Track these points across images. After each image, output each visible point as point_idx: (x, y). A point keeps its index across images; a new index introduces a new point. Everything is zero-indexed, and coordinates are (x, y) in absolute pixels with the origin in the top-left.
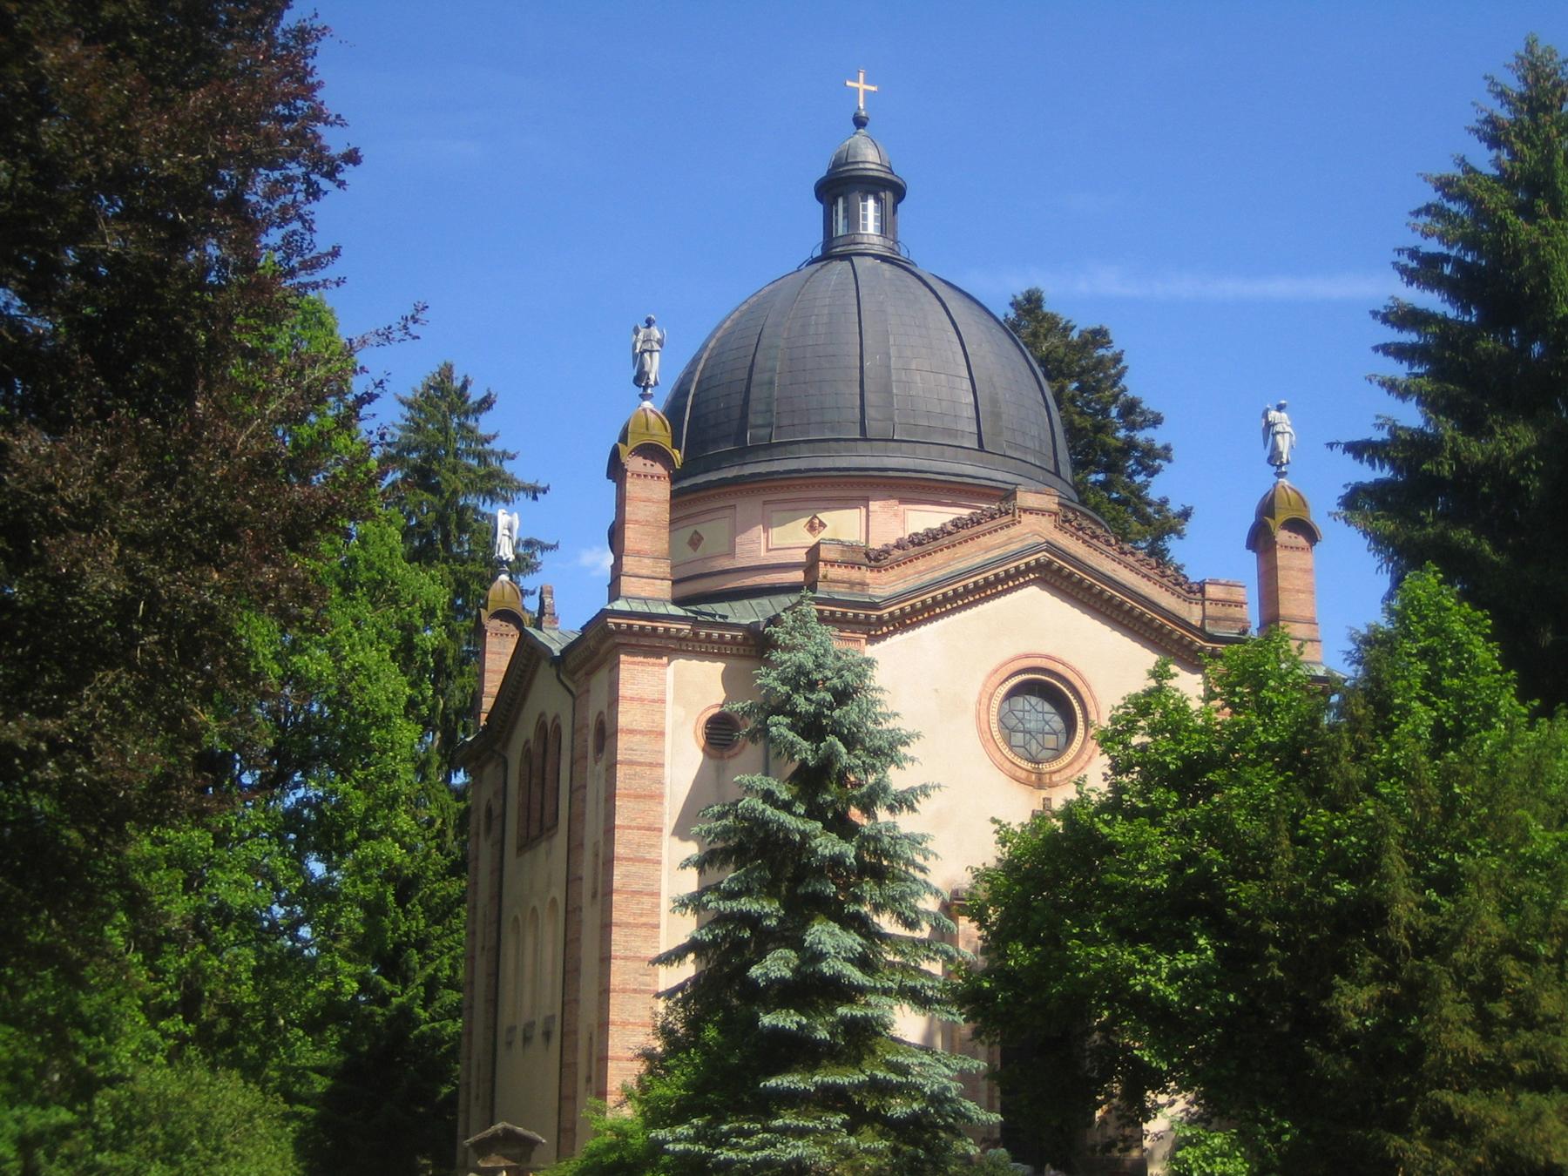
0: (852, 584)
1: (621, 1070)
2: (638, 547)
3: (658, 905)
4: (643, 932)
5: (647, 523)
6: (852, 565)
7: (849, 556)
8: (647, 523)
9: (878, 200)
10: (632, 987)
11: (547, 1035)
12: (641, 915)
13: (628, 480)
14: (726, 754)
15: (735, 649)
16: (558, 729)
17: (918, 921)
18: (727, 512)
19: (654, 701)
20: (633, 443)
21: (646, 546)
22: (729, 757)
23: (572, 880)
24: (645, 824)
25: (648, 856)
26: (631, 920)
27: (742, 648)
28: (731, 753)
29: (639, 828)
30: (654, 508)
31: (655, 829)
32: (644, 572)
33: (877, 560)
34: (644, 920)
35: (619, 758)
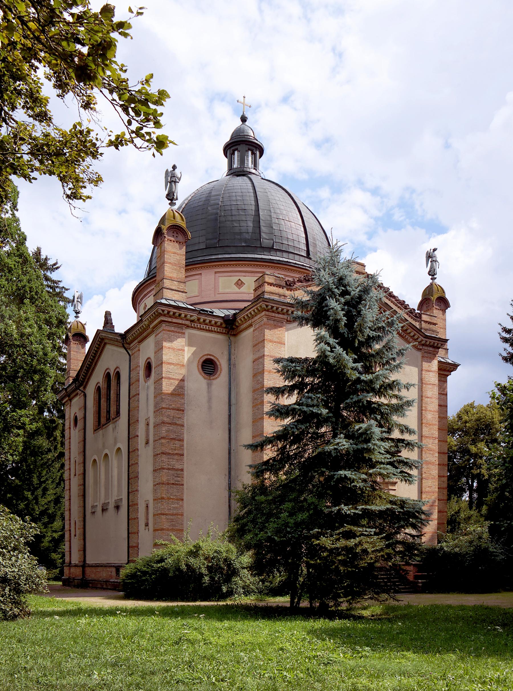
0: (280, 296)
1: (168, 519)
2: (171, 275)
3: (183, 446)
4: (176, 457)
5: (175, 265)
6: (279, 286)
7: (278, 282)
8: (175, 265)
9: (253, 153)
10: (172, 482)
11: (117, 507)
12: (175, 450)
13: (166, 242)
14: (212, 378)
15: (216, 328)
16: (118, 375)
17: (381, 433)
18: (197, 277)
19: (179, 350)
20: (168, 224)
21: (174, 275)
22: (213, 379)
23: (131, 437)
24: (176, 407)
25: (177, 422)
26: (170, 452)
27: (219, 329)
28: (214, 377)
29: (173, 409)
30: (178, 257)
31: (180, 410)
32: (174, 288)
33: (290, 285)
34: (176, 452)
35: (164, 375)
